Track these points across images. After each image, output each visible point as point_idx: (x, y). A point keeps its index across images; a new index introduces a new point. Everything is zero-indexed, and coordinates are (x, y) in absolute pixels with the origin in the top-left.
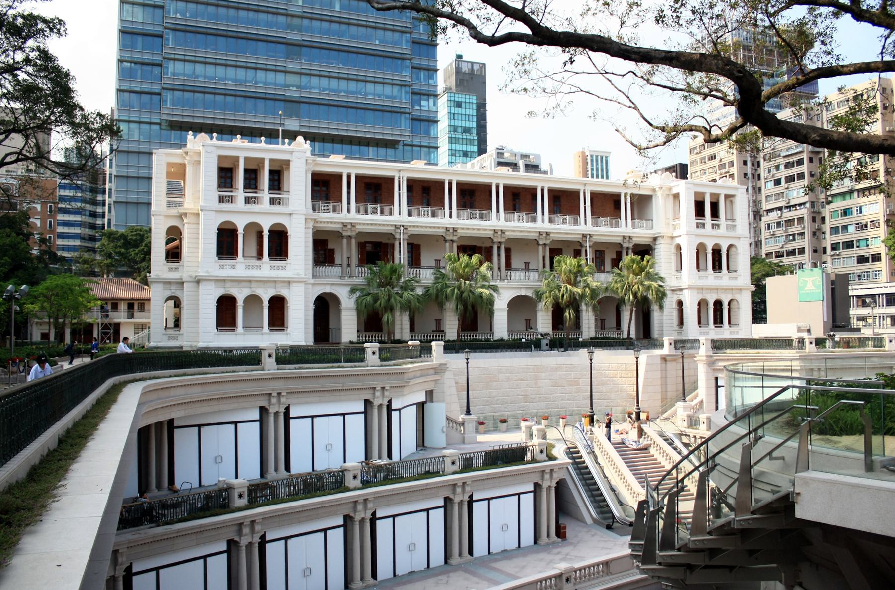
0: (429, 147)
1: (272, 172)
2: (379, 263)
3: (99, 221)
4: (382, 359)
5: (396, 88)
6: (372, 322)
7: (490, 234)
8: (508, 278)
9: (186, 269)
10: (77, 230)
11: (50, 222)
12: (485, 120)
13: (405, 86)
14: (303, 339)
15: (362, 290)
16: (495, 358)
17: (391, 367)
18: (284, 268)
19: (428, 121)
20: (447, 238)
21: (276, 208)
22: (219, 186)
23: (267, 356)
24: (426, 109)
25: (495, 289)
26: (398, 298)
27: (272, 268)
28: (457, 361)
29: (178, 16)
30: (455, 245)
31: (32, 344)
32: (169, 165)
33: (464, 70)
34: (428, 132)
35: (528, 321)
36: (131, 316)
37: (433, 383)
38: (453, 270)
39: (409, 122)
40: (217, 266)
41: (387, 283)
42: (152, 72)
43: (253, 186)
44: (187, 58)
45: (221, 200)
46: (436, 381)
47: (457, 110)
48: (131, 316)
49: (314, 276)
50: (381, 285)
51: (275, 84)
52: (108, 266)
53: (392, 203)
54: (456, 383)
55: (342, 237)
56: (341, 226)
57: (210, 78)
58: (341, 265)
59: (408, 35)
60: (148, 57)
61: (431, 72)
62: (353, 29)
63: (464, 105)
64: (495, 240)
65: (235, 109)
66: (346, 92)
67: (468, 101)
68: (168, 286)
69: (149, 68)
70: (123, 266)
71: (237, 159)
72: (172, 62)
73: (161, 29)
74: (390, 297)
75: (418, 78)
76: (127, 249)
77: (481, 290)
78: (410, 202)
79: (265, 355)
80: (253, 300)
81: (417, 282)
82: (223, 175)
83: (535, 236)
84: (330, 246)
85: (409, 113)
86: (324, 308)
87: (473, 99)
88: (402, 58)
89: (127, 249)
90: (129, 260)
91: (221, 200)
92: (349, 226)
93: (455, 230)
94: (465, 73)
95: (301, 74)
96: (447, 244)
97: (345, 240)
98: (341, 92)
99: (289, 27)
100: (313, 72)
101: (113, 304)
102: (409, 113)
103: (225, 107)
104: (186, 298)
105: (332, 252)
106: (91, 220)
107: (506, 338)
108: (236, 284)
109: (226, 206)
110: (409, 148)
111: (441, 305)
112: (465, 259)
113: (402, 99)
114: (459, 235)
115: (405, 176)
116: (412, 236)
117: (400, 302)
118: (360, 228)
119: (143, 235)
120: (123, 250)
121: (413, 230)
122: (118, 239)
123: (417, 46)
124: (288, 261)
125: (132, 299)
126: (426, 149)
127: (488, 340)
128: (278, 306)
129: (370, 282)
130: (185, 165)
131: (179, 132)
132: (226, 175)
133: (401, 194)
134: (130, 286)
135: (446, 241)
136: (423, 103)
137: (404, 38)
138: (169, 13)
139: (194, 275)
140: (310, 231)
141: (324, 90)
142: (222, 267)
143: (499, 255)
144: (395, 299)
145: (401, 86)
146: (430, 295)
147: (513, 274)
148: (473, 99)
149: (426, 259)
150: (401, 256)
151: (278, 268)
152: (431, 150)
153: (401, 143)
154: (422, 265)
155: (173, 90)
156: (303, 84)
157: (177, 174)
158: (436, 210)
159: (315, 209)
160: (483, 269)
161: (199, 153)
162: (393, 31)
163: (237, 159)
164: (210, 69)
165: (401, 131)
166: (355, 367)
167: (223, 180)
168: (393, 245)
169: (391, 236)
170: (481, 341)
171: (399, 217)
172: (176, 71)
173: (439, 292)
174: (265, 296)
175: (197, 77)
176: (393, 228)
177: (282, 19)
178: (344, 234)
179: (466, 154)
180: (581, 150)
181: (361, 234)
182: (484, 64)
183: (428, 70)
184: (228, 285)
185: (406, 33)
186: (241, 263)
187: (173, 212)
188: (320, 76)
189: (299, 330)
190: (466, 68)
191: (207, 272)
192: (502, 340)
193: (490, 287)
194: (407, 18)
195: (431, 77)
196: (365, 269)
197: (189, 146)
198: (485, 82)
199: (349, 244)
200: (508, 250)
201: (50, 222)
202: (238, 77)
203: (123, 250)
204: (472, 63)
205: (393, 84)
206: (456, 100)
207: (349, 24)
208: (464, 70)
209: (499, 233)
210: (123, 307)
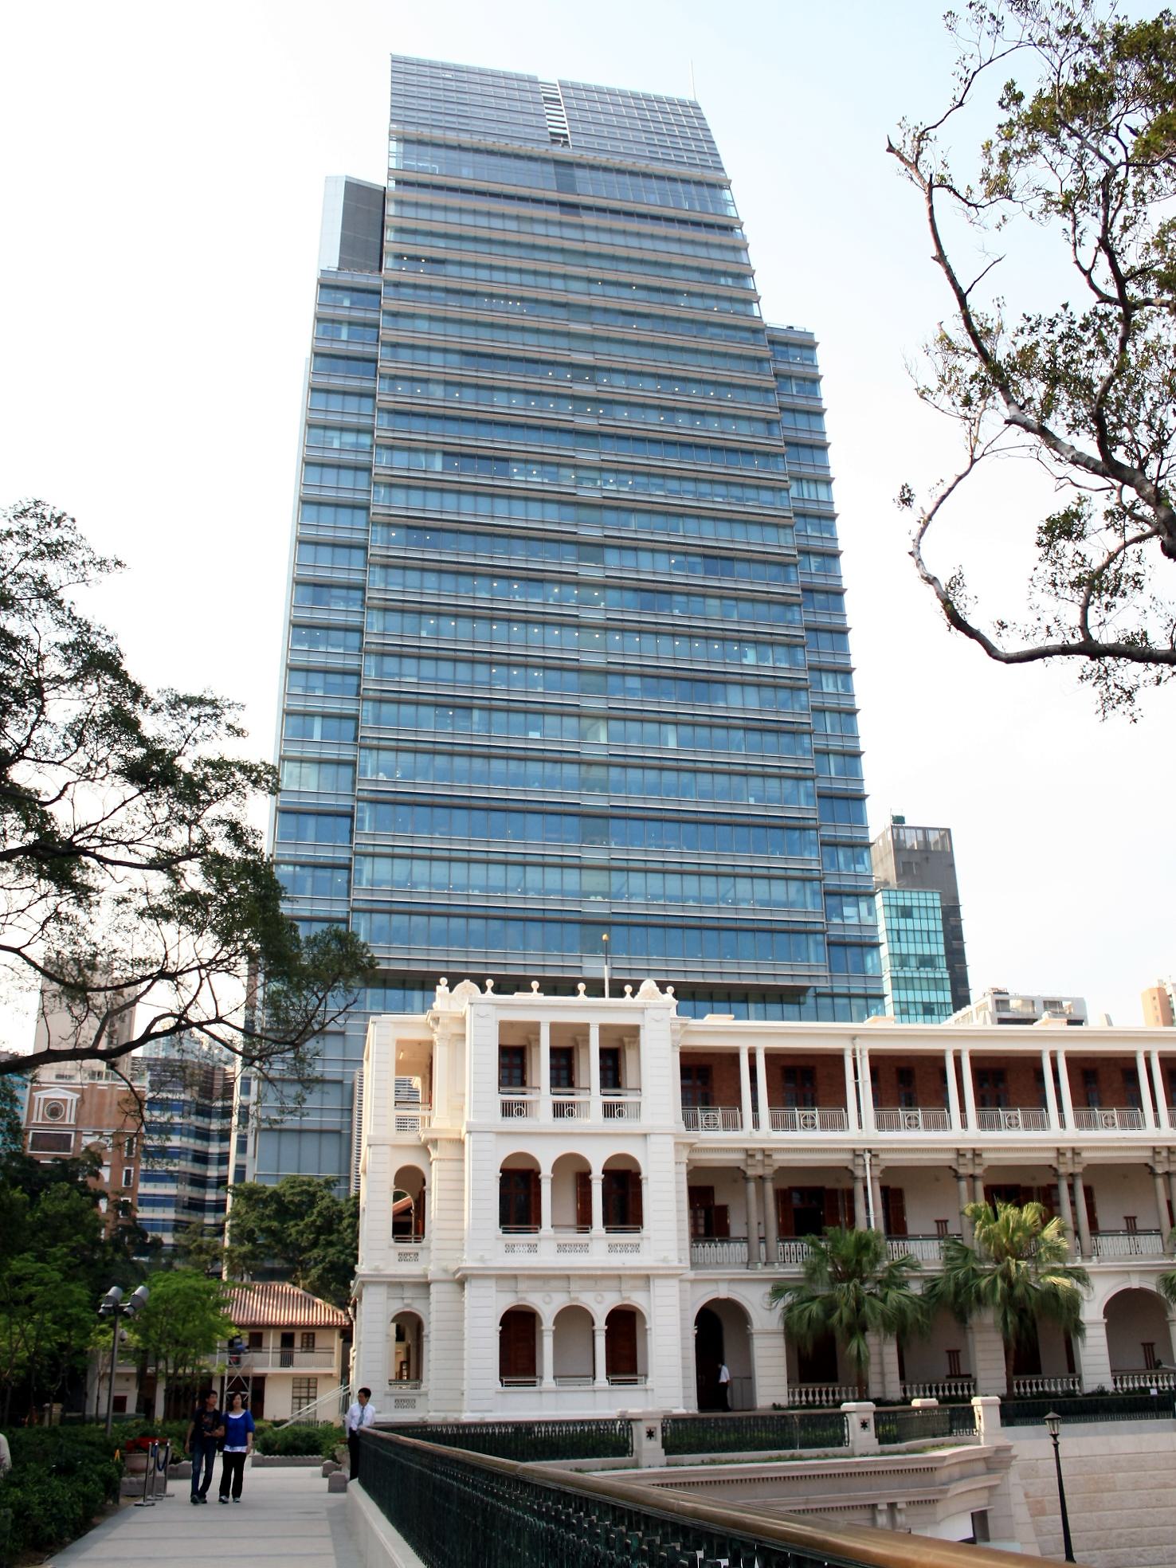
0: (866, 997)
1: (603, 1052)
2: (830, 1230)
3: (213, 1172)
4: (883, 1439)
5: (794, 886)
6: (818, 1358)
7: (1049, 1158)
8: (1095, 1251)
9: (434, 1255)
10: (170, 1189)
11: (128, 1172)
12: (960, 938)
13: (811, 880)
14: (679, 1401)
15: (799, 1289)
16: (1097, 1434)
17: (900, 1456)
18: (636, 1248)
19: (861, 945)
20: (962, 1171)
21: (615, 1124)
22: (501, 1084)
23: (644, 1434)
24: (855, 921)
25: (1081, 1276)
26: (879, 1305)
27: (612, 1248)
28: (1030, 1443)
29: (382, 776)
30: (980, 1186)
32: (401, 1045)
33: (908, 845)
34: (862, 968)
35: (1148, 1348)
36: (286, 1361)
37: (986, 1493)
38: (987, 1238)
39: (823, 950)
40: (501, 1246)
41: (852, 1270)
42: (332, 879)
43: (564, 1082)
44: (397, 851)
45: (507, 1110)
46: (991, 1488)
47: (903, 923)
48: (286, 1361)
49: (694, 1265)
50: (837, 1278)
51: (562, 892)
52: (244, 1257)
53: (843, 1104)
54: (1026, 1495)
55: (746, 1179)
56: (742, 1156)
57: (439, 886)
58: (746, 1240)
59: (809, 783)
60: (325, 854)
61: (857, 850)
62: (704, 780)
63: (915, 912)
64: (1062, 1170)
65: (488, 942)
66: (696, 899)
67: (923, 903)
68: (398, 1292)
69: (327, 873)
70: (275, 1256)
71: (535, 1027)
72: (369, 859)
73: (348, 802)
74: (859, 1302)
75: (834, 862)
76: (282, 1222)
77: (1053, 1279)
78: (878, 1102)
79: (640, 1431)
80: (574, 1317)
81: (913, 1267)
82: (507, 1060)
83: (1145, 1156)
84: (719, 1200)
85: (823, 933)
86: (717, 1329)
87: (934, 899)
88: (799, 827)
89: (282, 1222)
90: (286, 1246)
91: (507, 1110)
92: (759, 1157)
93: (977, 1154)
94: (912, 850)
95: (610, 869)
96: (963, 1184)
97: (752, 1186)
98: (687, 899)
99: (584, 784)
100: (632, 865)
101: (252, 1335)
102: (823, 933)
103: (466, 940)
104: (435, 1315)
105: (723, 1210)
106: (197, 1169)
107: (1109, 1387)
108: (539, 1283)
109: (515, 1123)
110: (828, 1001)
111: (962, 1316)
112: (1008, 1212)
113: (806, 906)
114: (987, 1164)
115: (865, 1047)
116: (889, 1171)
117: (883, 1313)
118: (781, 1160)
119: (314, 1195)
120: (275, 1224)
121: (888, 1159)
122: (265, 1203)
123: (827, 802)
124: (644, 1232)
125: (292, 1326)
126: (861, 1002)
127: (1070, 1394)
128: (625, 1327)
129: (812, 1273)
130: (430, 1044)
131: (380, 992)
132: (513, 1062)
133: (859, 1085)
134: (286, 1300)
135: (958, 1177)
136: (848, 911)
137: (802, 790)
138: (365, 773)
139: (453, 1267)
140: (684, 1169)
141: (655, 897)
142: (510, 1248)
143: (1073, 1203)
144: (873, 1307)
145: (804, 880)
146: (940, 1297)
147: (1105, 1242)
148: (934, 899)
149: (917, 1220)
150: (870, 1215)
151: (625, 1248)
152: (871, 1002)
153: (811, 992)
154: (911, 1231)
155: (371, 911)
156: (614, 889)
157: (420, 1061)
158: (933, 1113)
159: (691, 1123)
160: (1050, 1231)
161: (463, 1020)
162: (781, 777)
163: (535, 1027)
164: (440, 870)
165: (807, 966)
166: (827, 1456)
167: (506, 1072)
168: (850, 1195)
169: (847, 1172)
170: (1056, 1395)
171: (859, 1133)
172: (377, 877)
173: (961, 1287)
174: (600, 1308)
175: (414, 885)
176: (849, 1156)
177: (570, 771)
178: (750, 1172)
179: (928, 1009)
180: (1156, 985)
181: (783, 1171)
182: (948, 830)
183: (852, 846)
184: (522, 1285)
185: (805, 779)
186: (548, 1238)
187: (408, 1138)
188: (646, 871)
189: (668, 1382)
190: (912, 841)
191: (482, 1259)
192: (1102, 1392)
193: (1068, 1273)
194: (805, 752)
195: (858, 860)
196: (800, 1247)
197: (437, 1005)
198: (952, 866)
199: (761, 1193)
200: (1089, 1192)
201: (128, 1172)
202: (492, 883)
203: (275, 1224)
204: (925, 830)
205: (787, 879)
206: (901, 903)
207: (695, 771)
208: (908, 845)
209: (1069, 1155)
210: (272, 1341)
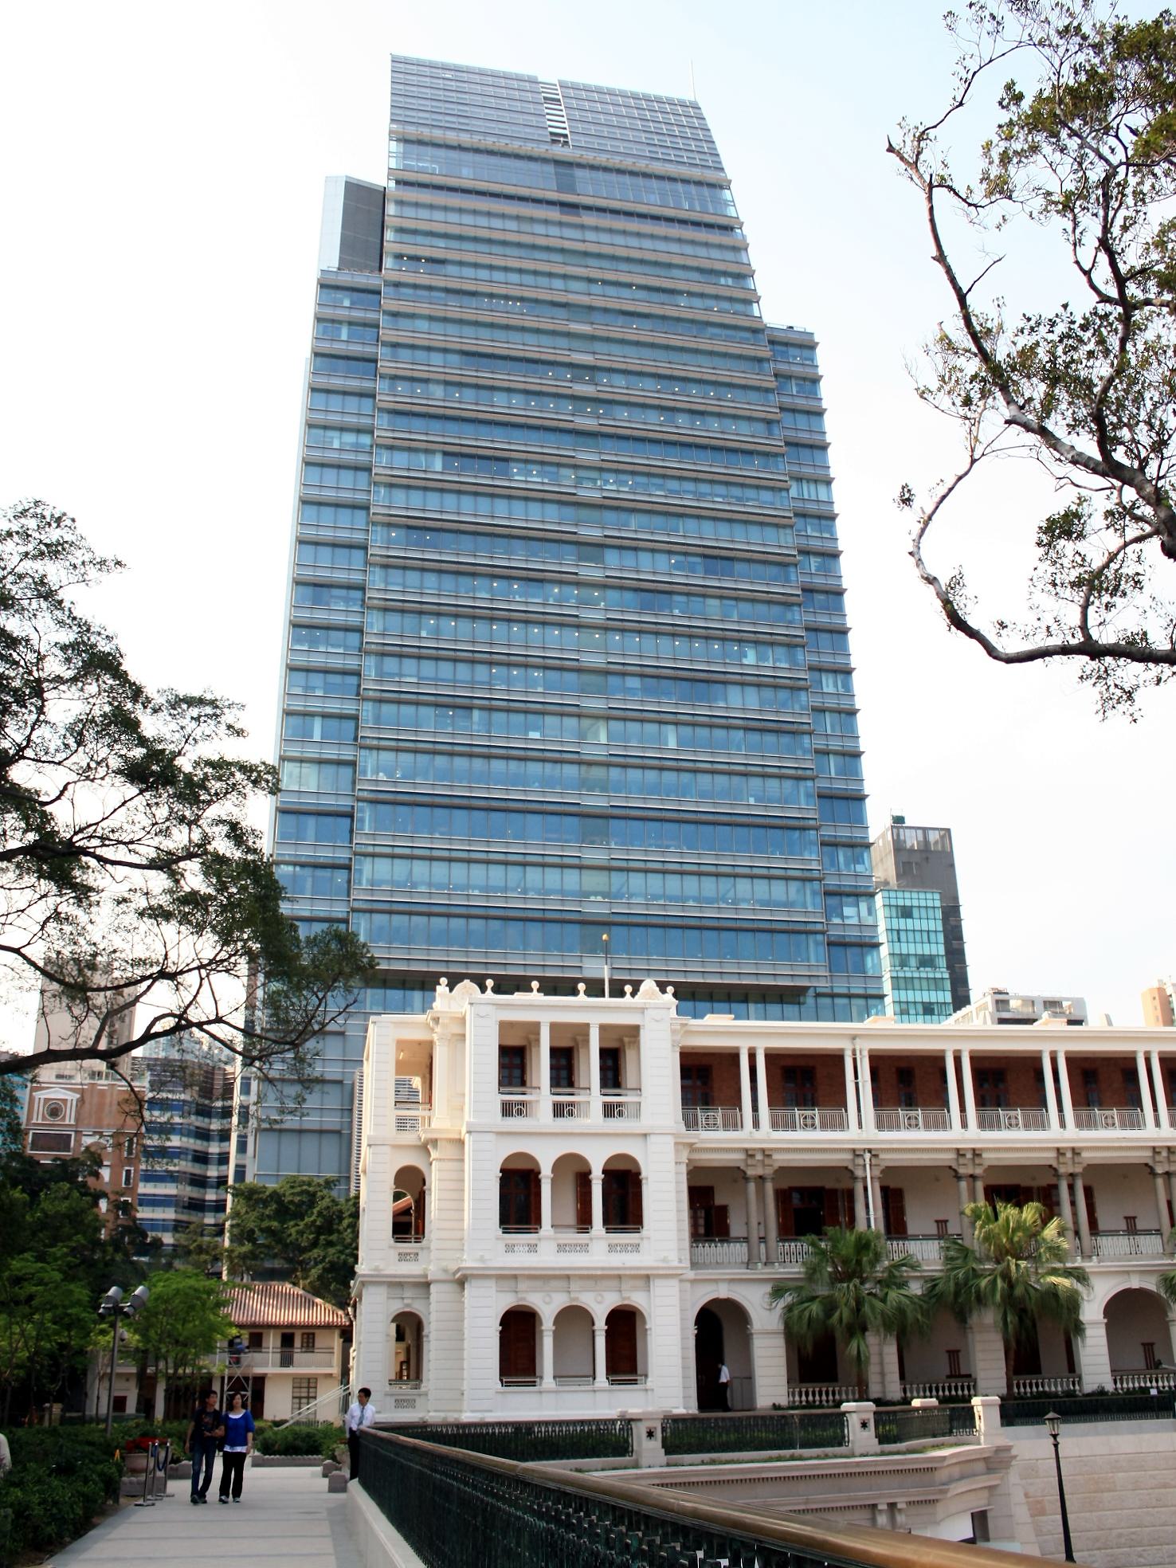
0: (866, 997)
1: (603, 1052)
2: (830, 1230)
3: (213, 1172)
4: (883, 1439)
5: (794, 886)
6: (818, 1358)
7: (1049, 1158)
8: (1095, 1251)
9: (434, 1255)
10: (170, 1189)
11: (128, 1172)
12: (960, 938)
13: (811, 880)
14: (679, 1401)
15: (799, 1289)
17: (900, 1456)
18: (636, 1248)
19: (861, 945)
20: (962, 1171)
21: (615, 1124)
22: (501, 1084)
23: (644, 1434)
24: (855, 921)
25: (1081, 1276)
26: (879, 1305)
27: (612, 1248)
29: (382, 776)
30: (980, 1186)
31: (98, 1420)
32: (401, 1045)
33: (908, 845)
34: (862, 968)
35: (1148, 1348)
36: (286, 1361)
38: (987, 1238)
39: (823, 950)
40: (501, 1246)
41: (852, 1270)
42: (332, 879)
43: (564, 1082)
44: (397, 851)
45: (507, 1110)
47: (903, 923)
48: (286, 1361)
49: (694, 1265)
50: (837, 1278)
51: (562, 892)
52: (244, 1257)
53: (843, 1104)
55: (746, 1179)
56: (742, 1156)
57: (439, 886)
58: (746, 1240)
59: (809, 783)
60: (325, 854)
61: (857, 850)
62: (704, 780)
63: (915, 912)
64: (1062, 1170)
65: (488, 942)
66: (696, 899)
67: (923, 903)
68: (398, 1292)
69: (327, 873)
70: (275, 1256)
71: (535, 1027)
72: (369, 859)
73: (348, 802)
74: (859, 1302)
75: (834, 862)
76: (282, 1222)
77: (1053, 1279)
78: (878, 1102)
79: (640, 1431)
80: (574, 1317)
81: (913, 1267)
82: (507, 1060)
83: (1145, 1156)
84: (719, 1200)
85: (823, 933)
86: (717, 1329)
87: (934, 899)
88: (799, 827)
89: (282, 1222)
90: (286, 1246)
91: (507, 1110)
92: (759, 1157)
93: (977, 1154)
94: (912, 850)
95: (610, 869)
96: (963, 1184)
97: (752, 1186)
98: (687, 899)
99: (584, 784)
100: (632, 865)
101: (252, 1335)
102: (823, 933)
103: (466, 940)
104: (435, 1315)
105: (723, 1210)
106: (197, 1169)
107: (1109, 1387)
108: (539, 1283)
109: (515, 1123)
110: (828, 1001)
111: (962, 1316)
112: (1008, 1212)
113: (806, 906)
114: (987, 1164)
115: (865, 1047)
116: (889, 1171)
117: (883, 1313)
118: (781, 1160)
119: (314, 1195)
120: (275, 1224)
121: (888, 1159)
122: (265, 1203)
123: (827, 802)
124: (644, 1232)
125: (292, 1326)
126: (861, 1002)
127: (1070, 1394)
128: (625, 1327)
129: (812, 1273)
130: (430, 1044)
131: (380, 992)
132: (513, 1062)
133: (859, 1085)
134: (286, 1300)
135: (958, 1177)
136: (848, 911)
137: (802, 790)
138: (365, 773)
139: (453, 1267)
140: (684, 1169)
141: (655, 897)
142: (510, 1248)
143: (1073, 1203)
144: (873, 1307)
145: (804, 880)
146: (940, 1297)
147: (1105, 1242)
148: (934, 899)
149: (917, 1220)
150: (870, 1215)
151: (625, 1248)
152: (871, 1002)
153: (811, 992)
154: (911, 1231)
155: (371, 911)
156: (614, 889)
157: (420, 1061)
158: (933, 1113)
159: (691, 1123)
160: (1050, 1231)
161: (463, 1020)
162: (781, 777)
163: (535, 1027)
164: (440, 870)
165: (807, 966)
166: (827, 1456)
167: (506, 1072)
168: (850, 1195)
169: (847, 1172)
170: (1056, 1395)
171: (859, 1133)
172: (377, 877)
173: (961, 1287)
174: (600, 1308)
175: (414, 885)
176: (849, 1156)
177: (570, 771)
178: (750, 1172)
179: (928, 1009)
180: (1156, 985)
181: (783, 1171)
182: (948, 830)
183: (852, 846)
184: (522, 1285)
185: (805, 779)
186: (548, 1238)
187: (408, 1138)
188: (646, 871)
189: (668, 1382)
190: (912, 841)
191: (482, 1259)
192: (1102, 1392)
193: (1068, 1273)
194: (805, 752)
195: (858, 860)
196: (800, 1247)
197: (437, 1005)
198: (952, 866)
199: (761, 1193)
200: (1089, 1192)
201: (128, 1172)
202: (492, 883)
203: (275, 1224)
204: (925, 830)
205: (787, 879)
206: (901, 903)
207: (695, 771)
208: (908, 845)
209: (1069, 1155)
210: (272, 1341)
